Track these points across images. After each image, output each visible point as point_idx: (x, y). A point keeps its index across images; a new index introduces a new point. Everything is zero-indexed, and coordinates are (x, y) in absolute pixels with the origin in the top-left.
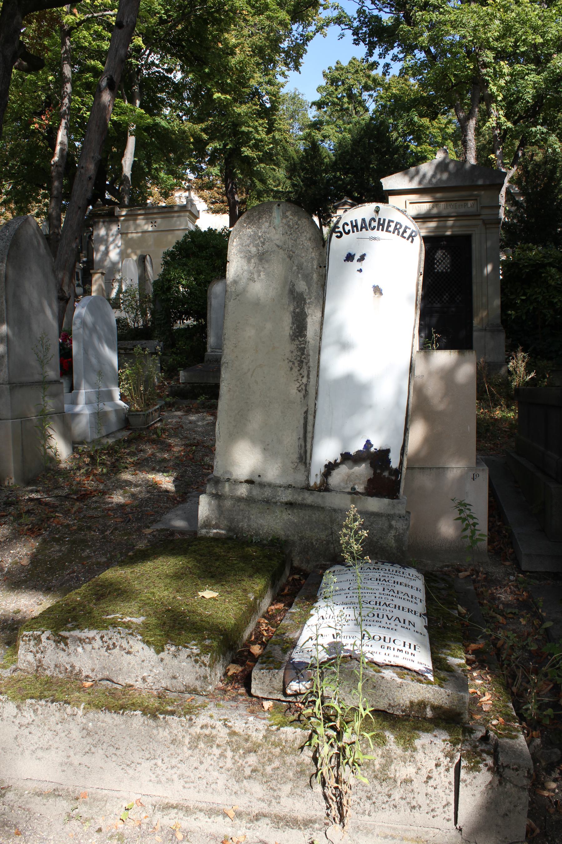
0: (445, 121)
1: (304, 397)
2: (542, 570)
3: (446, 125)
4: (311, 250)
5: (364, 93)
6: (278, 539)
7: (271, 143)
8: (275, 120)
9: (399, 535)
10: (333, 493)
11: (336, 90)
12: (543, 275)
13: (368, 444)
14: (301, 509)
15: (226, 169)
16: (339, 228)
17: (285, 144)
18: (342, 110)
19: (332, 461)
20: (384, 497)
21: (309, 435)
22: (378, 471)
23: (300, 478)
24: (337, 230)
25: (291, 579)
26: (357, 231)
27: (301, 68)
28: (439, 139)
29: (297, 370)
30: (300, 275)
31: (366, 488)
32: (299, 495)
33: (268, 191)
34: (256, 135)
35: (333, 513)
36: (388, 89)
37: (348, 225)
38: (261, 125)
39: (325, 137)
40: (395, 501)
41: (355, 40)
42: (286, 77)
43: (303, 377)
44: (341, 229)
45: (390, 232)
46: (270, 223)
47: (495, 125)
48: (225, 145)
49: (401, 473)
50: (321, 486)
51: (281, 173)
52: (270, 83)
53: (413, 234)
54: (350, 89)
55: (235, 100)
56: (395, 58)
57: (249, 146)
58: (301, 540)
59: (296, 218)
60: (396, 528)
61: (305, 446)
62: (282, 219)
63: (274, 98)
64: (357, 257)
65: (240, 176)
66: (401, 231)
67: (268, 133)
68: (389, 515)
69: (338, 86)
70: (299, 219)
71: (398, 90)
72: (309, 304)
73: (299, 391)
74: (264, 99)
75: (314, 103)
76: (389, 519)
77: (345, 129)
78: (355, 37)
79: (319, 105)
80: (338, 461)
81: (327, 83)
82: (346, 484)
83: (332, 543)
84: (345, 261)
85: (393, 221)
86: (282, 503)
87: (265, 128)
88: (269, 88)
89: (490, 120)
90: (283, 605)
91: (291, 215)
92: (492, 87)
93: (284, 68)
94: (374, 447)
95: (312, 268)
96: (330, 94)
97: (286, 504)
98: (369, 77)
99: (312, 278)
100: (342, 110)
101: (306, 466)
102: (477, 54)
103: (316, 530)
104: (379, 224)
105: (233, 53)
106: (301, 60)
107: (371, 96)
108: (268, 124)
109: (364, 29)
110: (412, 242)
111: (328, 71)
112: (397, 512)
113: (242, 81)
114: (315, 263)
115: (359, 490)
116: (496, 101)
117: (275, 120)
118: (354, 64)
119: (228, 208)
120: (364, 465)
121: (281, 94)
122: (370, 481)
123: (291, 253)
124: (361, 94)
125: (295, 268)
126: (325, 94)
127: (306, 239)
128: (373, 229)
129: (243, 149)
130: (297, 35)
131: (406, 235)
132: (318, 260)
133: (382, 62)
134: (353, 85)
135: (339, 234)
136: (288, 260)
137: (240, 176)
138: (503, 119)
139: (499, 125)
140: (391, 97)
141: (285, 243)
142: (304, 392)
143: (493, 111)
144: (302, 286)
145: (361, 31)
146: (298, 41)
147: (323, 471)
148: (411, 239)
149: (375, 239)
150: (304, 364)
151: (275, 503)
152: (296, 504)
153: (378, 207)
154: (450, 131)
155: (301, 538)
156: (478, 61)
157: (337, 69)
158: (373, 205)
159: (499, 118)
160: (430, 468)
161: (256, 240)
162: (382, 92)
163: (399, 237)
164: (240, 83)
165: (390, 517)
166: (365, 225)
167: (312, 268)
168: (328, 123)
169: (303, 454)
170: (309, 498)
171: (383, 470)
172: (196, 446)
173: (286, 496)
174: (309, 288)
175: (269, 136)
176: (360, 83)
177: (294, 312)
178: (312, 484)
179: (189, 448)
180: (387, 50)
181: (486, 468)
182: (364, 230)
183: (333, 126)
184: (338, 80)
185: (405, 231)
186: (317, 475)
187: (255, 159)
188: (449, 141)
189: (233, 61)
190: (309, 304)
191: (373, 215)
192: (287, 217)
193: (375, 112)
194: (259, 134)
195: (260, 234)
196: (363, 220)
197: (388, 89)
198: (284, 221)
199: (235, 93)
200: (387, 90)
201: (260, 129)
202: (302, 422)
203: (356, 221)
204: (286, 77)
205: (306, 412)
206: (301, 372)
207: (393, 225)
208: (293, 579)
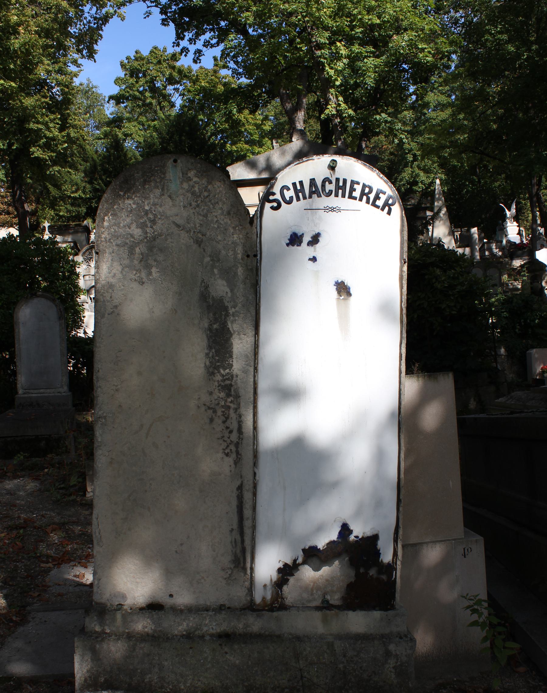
0: (261, 117)
1: (236, 463)
3: (262, 121)
4: (232, 231)
5: (168, 87)
7: (65, 142)
8: (69, 115)
11: (137, 82)
12: (426, 277)
13: (345, 530)
15: (12, 173)
16: (274, 194)
17: (82, 142)
18: (144, 105)
20: (374, 608)
21: (247, 523)
22: (362, 570)
24: (271, 198)
26: (305, 198)
27: (96, 56)
28: (256, 137)
29: (220, 422)
30: (216, 271)
31: (343, 599)
33: (64, 198)
34: (46, 132)
36: (195, 81)
37: (288, 189)
38: (52, 121)
39: (126, 135)
40: (391, 613)
41: (163, 20)
42: (79, 66)
43: (231, 432)
44: (278, 196)
45: (355, 198)
46: (163, 189)
47: (334, 112)
48: (10, 145)
49: (396, 569)
50: (273, 602)
51: (78, 177)
52: (60, 71)
53: (390, 202)
54: (152, 81)
55: (21, 89)
56: (207, 44)
57: (39, 146)
59: (204, 181)
60: (397, 655)
61: (243, 541)
62: (182, 183)
63: (66, 90)
64: (307, 239)
65: (29, 181)
66: (372, 196)
67: (61, 130)
68: (382, 636)
69: (139, 78)
70: (209, 183)
71: (207, 82)
72: (233, 315)
73: (227, 455)
74: (54, 90)
75: (111, 98)
77: (149, 126)
78: (164, 17)
79: (118, 99)
81: (126, 75)
84: (288, 245)
85: (358, 183)
86: (212, 635)
87: (58, 124)
88: (59, 77)
89: (329, 107)
91: (196, 176)
92: (329, 70)
93: (76, 56)
94: (355, 533)
95: (235, 258)
96: (131, 87)
98: (173, 68)
99: (236, 274)
100: (144, 105)
102: (309, 34)
104: (338, 187)
105: (16, 33)
106: (95, 47)
107: (176, 90)
108: (60, 119)
109: (174, 7)
110: (389, 213)
111: (126, 61)
113: (29, 66)
114: (240, 250)
115: (331, 602)
116: (333, 86)
117: (69, 115)
118: (156, 54)
119: (16, 220)
120: (337, 563)
121: (74, 84)
122: (350, 587)
123: (200, 235)
124: (166, 87)
125: (207, 259)
126: (123, 87)
127: (222, 214)
128: (329, 194)
129: (33, 149)
130: (89, 18)
131: (380, 203)
132: (244, 246)
133: (192, 48)
134: (156, 77)
135: (275, 204)
136: (195, 246)
137: (29, 181)
138: (343, 106)
139: (339, 113)
140: (200, 90)
141: (188, 221)
142: (234, 455)
143: (331, 97)
144: (220, 288)
145: (170, 10)
146: (92, 25)
148: (387, 208)
149: (333, 209)
150: (232, 411)
151: (202, 637)
153: (334, 161)
154: (267, 127)
156: (311, 42)
157: (136, 59)
158: (326, 159)
159: (339, 105)
161: (142, 217)
162: (189, 84)
163: (369, 206)
164: (26, 68)
166: (316, 189)
167: (235, 258)
168: (129, 120)
172: (24, 528)
173: (213, 625)
174: (232, 291)
175: (63, 134)
176: (164, 75)
177: (210, 329)
178: (258, 599)
179: (15, 532)
180: (197, 35)
181: (481, 539)
182: (314, 196)
183: (135, 123)
184: (139, 71)
185: (377, 197)
187: (47, 161)
188: (267, 139)
189: (16, 43)
190: (233, 315)
191: (327, 173)
192: (190, 179)
193: (182, 107)
194: (51, 132)
195: (147, 208)
196: (313, 182)
197: (195, 81)
198: (185, 186)
199: (21, 80)
200: (194, 84)
201: (51, 125)
202: (234, 503)
203: (301, 183)
204: (79, 66)
205: (240, 488)
206: (228, 423)
207: (358, 188)
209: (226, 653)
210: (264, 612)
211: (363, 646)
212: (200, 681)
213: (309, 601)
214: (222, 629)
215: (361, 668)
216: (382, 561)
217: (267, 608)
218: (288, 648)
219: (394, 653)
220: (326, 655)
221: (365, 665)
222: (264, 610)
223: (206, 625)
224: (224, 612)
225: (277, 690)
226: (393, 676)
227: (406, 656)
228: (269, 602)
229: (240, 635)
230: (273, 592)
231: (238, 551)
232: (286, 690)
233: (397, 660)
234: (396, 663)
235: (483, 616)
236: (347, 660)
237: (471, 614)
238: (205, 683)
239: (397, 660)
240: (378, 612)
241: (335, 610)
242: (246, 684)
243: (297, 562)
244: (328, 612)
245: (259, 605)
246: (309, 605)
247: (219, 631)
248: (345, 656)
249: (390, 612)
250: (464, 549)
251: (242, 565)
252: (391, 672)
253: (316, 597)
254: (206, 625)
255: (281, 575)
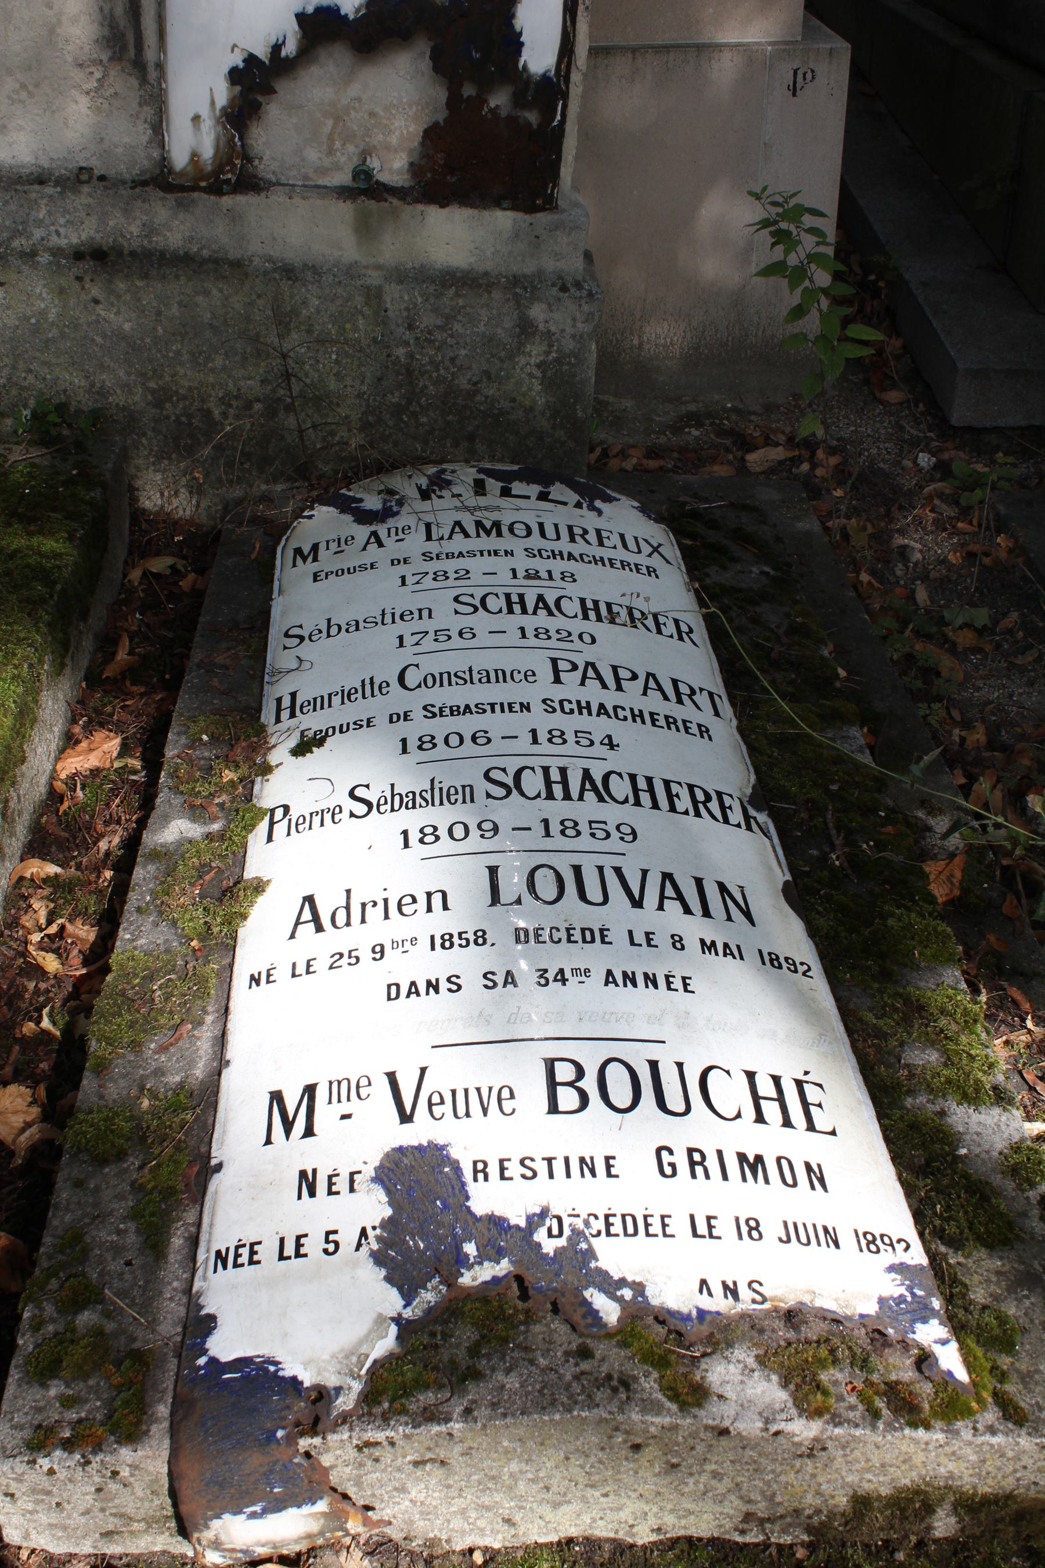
2: (1019, 421)
6: (62, 408)
9: (557, 360)
10: (277, 197)
14: (146, 276)
19: (262, 52)
20: (497, 203)
22: (468, 90)
23: (126, 141)
25: (135, 575)
31: (415, 169)
32: (127, 212)
35: (285, 285)
40: (543, 218)
49: (565, 96)
50: (219, 169)
58: (159, 404)
60: (549, 334)
68: (516, 281)
76: (517, 298)
80: (290, 49)
82: (331, 152)
83: (289, 408)
86: (57, 252)
90: (114, 744)
97: (78, 255)
101: (144, 80)
103: (219, 361)
112: (550, 265)
115: (384, 177)
147: (222, 99)
151: (30, 255)
152: (120, 253)
155: (161, 398)
160: (634, 50)
165: (521, 287)
169: (123, 22)
170: (175, 227)
171: (486, 86)
178: (180, 159)
181: (844, 48)
186: (196, 119)
208: (146, 574)
209: (96, 302)
210: (196, 195)
211: (461, 302)
212: (30, 371)
213: (323, 171)
214: (84, 237)
215: (452, 360)
216: (525, 66)
217: (203, 184)
218: (259, 296)
219: (541, 327)
220: (361, 321)
221: (463, 352)
222: (195, 188)
223: (39, 223)
224: (86, 189)
225: (234, 403)
226: (537, 387)
227: (573, 336)
228: (209, 168)
229: (133, 254)
230: (218, 139)
231: (119, 11)
232: (258, 406)
233: (550, 346)
234: (547, 353)
235: (799, 248)
236: (417, 339)
237: (774, 245)
238: (44, 379)
239: (550, 346)
240: (509, 213)
241: (390, 199)
242: (152, 385)
243: (283, 54)
244: (372, 204)
245: (182, 173)
246: (320, 182)
247: (75, 241)
248: (410, 327)
249: (539, 215)
250: (795, 72)
251: (132, 52)
252: (531, 375)
253: (343, 159)
254: (39, 223)
255: (238, 88)
